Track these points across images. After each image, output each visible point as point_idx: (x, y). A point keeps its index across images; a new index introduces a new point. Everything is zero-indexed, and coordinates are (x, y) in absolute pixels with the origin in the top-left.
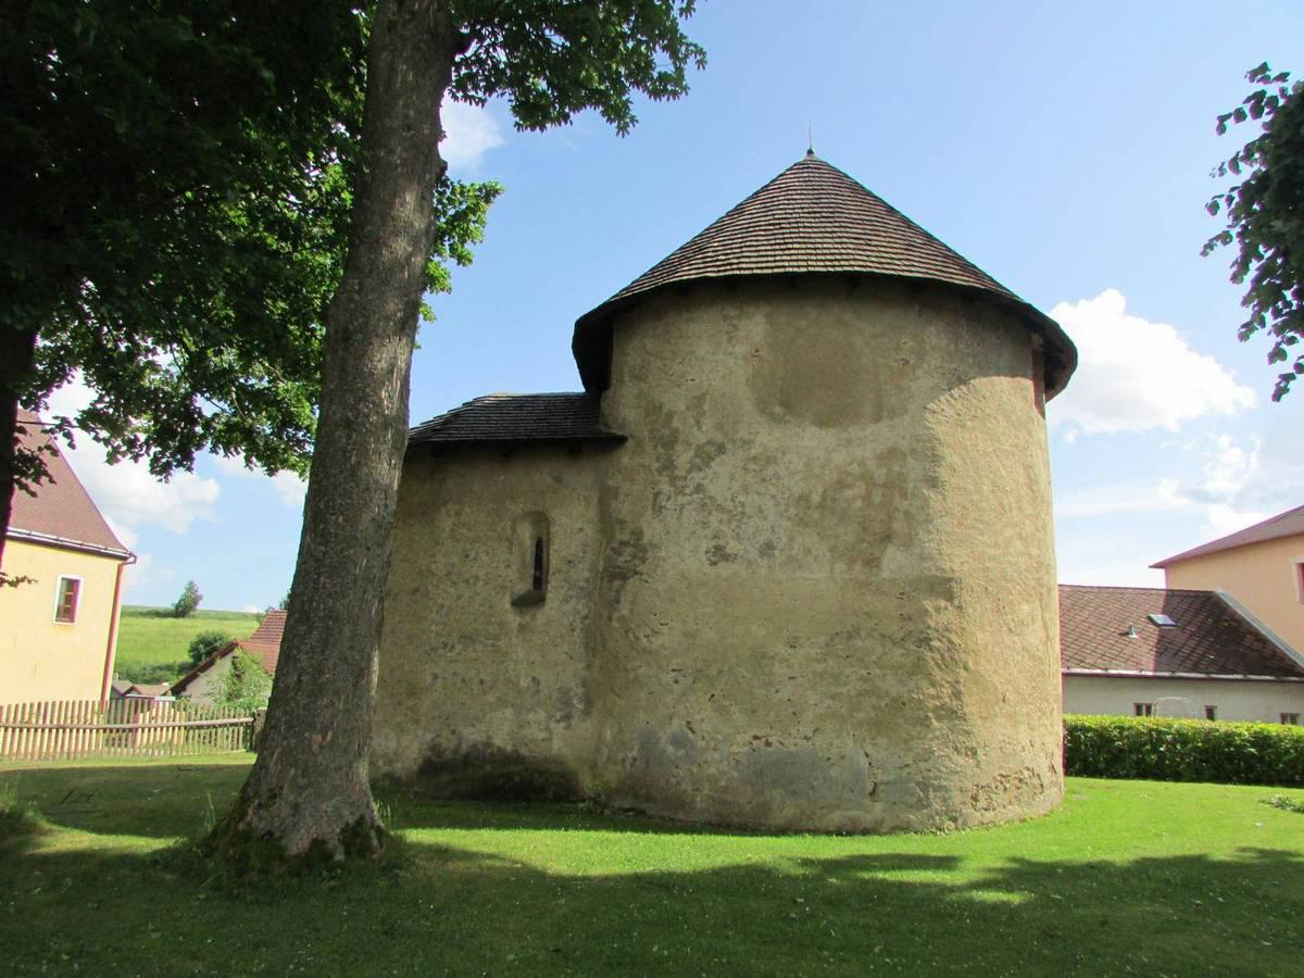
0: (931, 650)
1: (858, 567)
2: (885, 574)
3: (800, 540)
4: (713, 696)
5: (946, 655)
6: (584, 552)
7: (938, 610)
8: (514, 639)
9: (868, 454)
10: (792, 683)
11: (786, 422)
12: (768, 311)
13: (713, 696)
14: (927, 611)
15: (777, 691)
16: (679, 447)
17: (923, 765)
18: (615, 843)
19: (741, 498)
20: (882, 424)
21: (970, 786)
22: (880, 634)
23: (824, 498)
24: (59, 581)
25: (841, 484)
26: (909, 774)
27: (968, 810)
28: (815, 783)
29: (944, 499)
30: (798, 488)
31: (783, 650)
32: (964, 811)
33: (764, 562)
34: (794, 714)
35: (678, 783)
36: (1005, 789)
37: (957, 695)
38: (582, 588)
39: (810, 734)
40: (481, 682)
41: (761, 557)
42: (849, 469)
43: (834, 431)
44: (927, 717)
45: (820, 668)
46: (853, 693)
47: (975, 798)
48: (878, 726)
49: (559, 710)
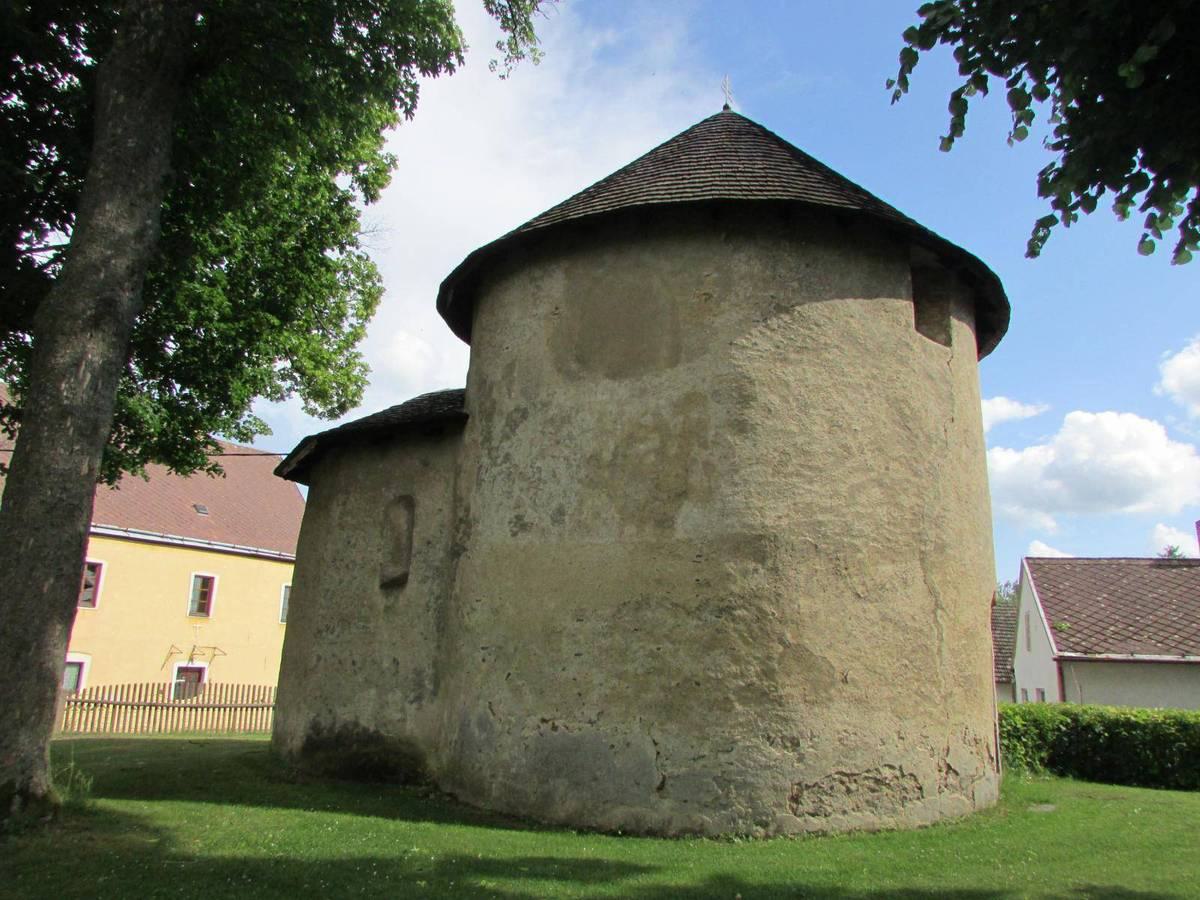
0: (733, 620)
1: (648, 529)
2: (680, 534)
3: (590, 503)
4: (509, 674)
5: (755, 626)
6: (441, 532)
7: (745, 573)
8: (381, 620)
9: (662, 402)
10: (579, 659)
11: (579, 379)
12: (567, 266)
13: (509, 674)
14: (729, 574)
15: (564, 669)
16: (496, 418)
17: (723, 758)
18: (363, 831)
19: (538, 464)
20: (681, 368)
21: (788, 784)
22: (672, 604)
23: (615, 455)
24: (283, 588)
25: (631, 439)
26: (705, 766)
27: (784, 814)
28: (598, 773)
29: (755, 445)
30: (590, 446)
31: (571, 625)
32: (778, 815)
33: (555, 530)
34: (580, 695)
35: (481, 769)
36: (849, 791)
37: (768, 673)
38: (437, 568)
39: (594, 718)
40: (354, 663)
41: (553, 525)
42: (642, 421)
43: (627, 382)
44: (727, 699)
45: (605, 642)
46: (640, 671)
47: (795, 799)
48: (669, 709)
49: (413, 690)
